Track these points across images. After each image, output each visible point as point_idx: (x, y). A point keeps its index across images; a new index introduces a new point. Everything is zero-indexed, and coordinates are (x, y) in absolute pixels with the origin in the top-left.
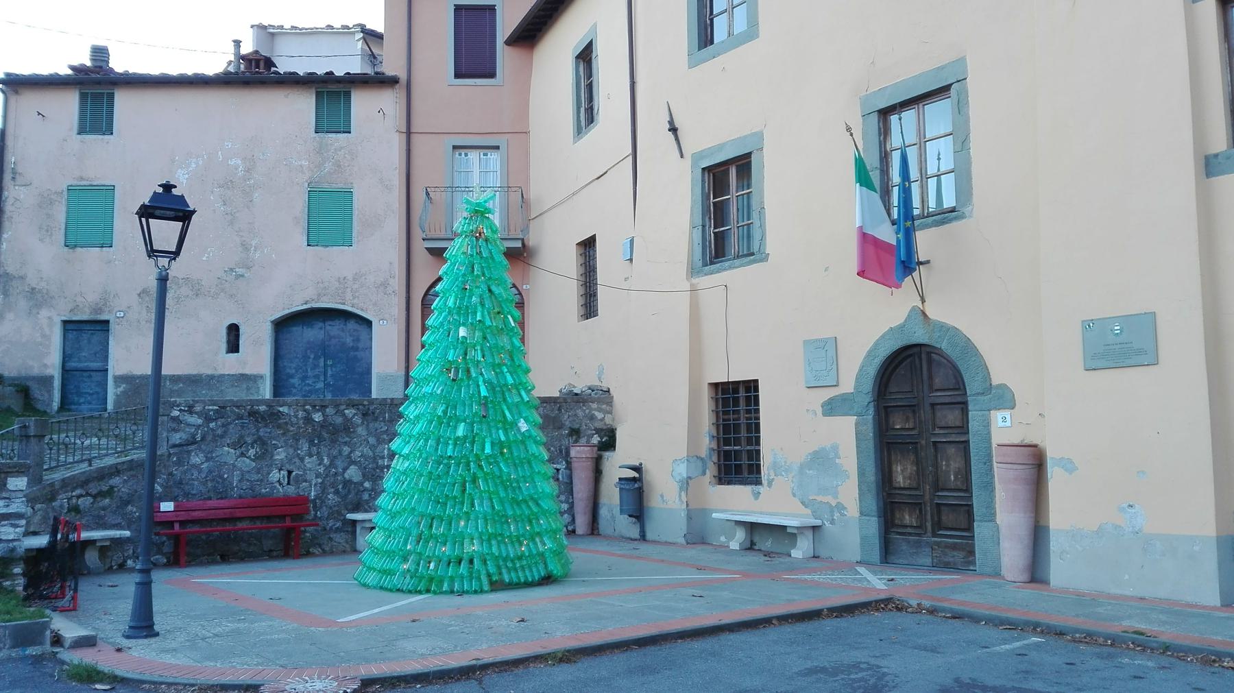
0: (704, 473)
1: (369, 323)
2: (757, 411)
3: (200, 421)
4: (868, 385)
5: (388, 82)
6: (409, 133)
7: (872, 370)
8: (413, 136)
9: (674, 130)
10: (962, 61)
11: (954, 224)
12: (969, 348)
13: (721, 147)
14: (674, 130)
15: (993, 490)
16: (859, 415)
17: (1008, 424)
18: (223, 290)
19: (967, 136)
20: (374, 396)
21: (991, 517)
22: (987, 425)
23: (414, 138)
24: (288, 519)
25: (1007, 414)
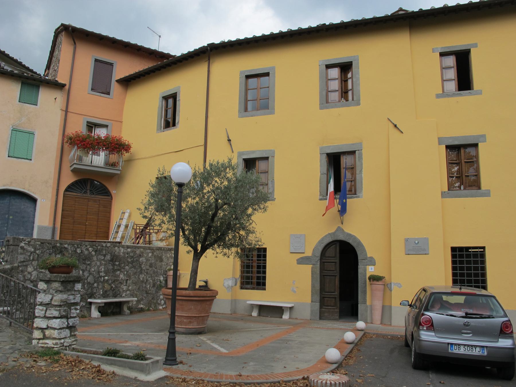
0: (236, 285)
1: (34, 200)
2: (265, 260)
3: (33, 250)
4: (318, 254)
5: (58, 86)
6: (67, 111)
7: (320, 249)
8: (68, 113)
9: (229, 140)
10: (361, 144)
11: (355, 199)
12: (360, 243)
13: (253, 152)
14: (229, 140)
15: (366, 293)
16: (313, 265)
17: (373, 270)
18: (225, 176)
19: (362, 170)
20: (35, 236)
21: (365, 302)
22: (365, 270)
23: (69, 114)
24: (462, 347)
25: (373, 267)
